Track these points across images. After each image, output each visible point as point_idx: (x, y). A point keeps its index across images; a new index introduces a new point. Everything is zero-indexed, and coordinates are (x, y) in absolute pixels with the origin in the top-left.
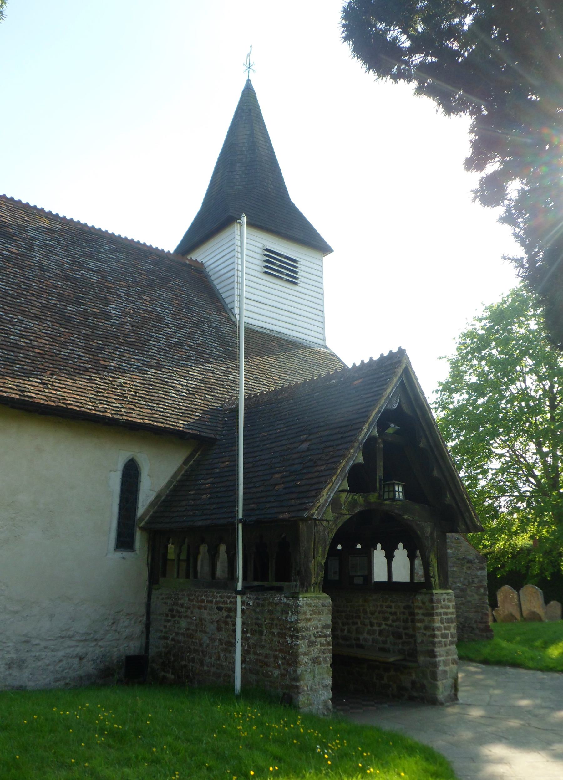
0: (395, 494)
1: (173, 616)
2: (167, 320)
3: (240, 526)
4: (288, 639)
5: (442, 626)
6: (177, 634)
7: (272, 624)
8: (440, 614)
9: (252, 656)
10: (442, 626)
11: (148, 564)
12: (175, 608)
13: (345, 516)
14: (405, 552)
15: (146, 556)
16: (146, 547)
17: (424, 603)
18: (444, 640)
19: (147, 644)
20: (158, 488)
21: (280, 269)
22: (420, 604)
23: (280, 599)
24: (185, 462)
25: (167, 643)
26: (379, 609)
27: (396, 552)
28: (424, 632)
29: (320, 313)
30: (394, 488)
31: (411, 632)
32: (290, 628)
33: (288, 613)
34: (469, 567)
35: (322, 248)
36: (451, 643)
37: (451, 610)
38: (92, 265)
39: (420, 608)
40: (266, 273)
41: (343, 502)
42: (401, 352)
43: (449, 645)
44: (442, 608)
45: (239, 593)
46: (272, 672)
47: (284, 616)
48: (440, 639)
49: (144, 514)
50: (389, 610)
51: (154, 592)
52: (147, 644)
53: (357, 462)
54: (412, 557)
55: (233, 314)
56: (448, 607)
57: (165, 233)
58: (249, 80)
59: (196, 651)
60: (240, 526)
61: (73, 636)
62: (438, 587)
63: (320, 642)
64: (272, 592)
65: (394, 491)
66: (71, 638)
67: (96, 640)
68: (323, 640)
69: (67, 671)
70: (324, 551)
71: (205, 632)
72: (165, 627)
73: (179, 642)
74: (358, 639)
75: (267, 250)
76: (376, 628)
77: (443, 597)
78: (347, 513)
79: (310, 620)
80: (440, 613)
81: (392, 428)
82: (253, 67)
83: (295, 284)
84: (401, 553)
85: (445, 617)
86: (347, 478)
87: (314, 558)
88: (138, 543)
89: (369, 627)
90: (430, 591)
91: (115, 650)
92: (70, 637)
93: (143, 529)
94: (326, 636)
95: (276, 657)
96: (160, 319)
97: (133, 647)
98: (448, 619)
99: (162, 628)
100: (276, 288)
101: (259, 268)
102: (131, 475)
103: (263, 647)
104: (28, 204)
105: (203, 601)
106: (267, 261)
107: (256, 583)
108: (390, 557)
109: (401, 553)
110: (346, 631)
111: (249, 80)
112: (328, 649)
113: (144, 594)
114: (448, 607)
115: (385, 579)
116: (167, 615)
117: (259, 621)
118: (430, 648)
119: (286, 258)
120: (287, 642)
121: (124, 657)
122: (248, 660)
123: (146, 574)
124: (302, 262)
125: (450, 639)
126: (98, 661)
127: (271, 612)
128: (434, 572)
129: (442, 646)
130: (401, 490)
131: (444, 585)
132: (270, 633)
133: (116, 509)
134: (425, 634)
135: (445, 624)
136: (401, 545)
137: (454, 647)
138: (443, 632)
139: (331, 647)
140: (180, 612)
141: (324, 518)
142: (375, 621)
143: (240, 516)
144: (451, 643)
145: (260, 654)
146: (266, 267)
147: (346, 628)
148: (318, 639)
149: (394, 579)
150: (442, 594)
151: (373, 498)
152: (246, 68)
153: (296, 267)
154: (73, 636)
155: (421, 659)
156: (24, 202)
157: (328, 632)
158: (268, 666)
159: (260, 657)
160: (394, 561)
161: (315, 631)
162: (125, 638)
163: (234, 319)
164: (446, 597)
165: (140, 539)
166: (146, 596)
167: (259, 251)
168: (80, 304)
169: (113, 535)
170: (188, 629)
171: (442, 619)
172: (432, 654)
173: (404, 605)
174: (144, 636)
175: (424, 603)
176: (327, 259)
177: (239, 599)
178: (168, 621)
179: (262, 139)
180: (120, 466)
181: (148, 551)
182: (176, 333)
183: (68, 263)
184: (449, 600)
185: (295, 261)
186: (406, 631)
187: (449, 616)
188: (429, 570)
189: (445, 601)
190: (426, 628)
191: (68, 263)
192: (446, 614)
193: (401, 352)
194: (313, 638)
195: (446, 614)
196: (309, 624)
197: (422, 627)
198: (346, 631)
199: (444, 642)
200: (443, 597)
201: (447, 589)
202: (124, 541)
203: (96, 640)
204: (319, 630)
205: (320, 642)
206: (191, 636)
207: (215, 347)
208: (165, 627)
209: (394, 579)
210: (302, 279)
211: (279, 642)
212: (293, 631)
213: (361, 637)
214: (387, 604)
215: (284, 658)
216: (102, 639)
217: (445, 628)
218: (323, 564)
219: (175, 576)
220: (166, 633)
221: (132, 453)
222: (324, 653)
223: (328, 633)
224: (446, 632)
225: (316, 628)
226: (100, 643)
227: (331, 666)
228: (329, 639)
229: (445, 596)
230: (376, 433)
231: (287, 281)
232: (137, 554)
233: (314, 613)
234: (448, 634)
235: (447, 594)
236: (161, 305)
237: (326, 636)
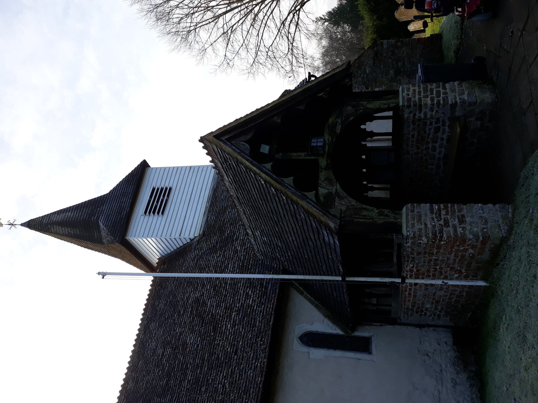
0: (319, 146)
1: (422, 311)
2: (197, 295)
3: (348, 279)
4: (442, 243)
5: (430, 96)
6: (436, 309)
7: (429, 253)
8: (420, 99)
9: (456, 266)
10: (430, 96)
11: (381, 325)
12: (415, 310)
13: (338, 188)
14: (368, 123)
15: (375, 327)
16: (367, 327)
17: (411, 112)
18: (442, 95)
19: (443, 327)
20: (322, 317)
21: (160, 201)
22: (412, 115)
23: (408, 247)
24: (302, 294)
25: (443, 315)
26: (415, 143)
27: (368, 130)
28: (434, 112)
29: (192, 170)
30: (314, 146)
31: (434, 121)
32: (432, 242)
33: (420, 243)
34: (381, 55)
35: (144, 166)
36: (444, 88)
37: (417, 88)
38: (160, 351)
39: (415, 115)
40: (163, 213)
41: (327, 191)
42: (202, 140)
43: (446, 89)
44: (414, 97)
45: (403, 281)
46: (470, 254)
47: (422, 245)
48: (441, 98)
49: (342, 329)
50: (416, 136)
51: (403, 321)
52: (443, 327)
53: (292, 184)
54: (372, 119)
55: (194, 239)
56: (414, 90)
57: (138, 287)
58: (22, 225)
59: (450, 299)
60: (348, 279)
61: (439, 391)
62: (397, 216)
63: (444, 215)
64: (402, 251)
65: (317, 146)
66: (440, 392)
67: (441, 371)
68: (443, 212)
69: (466, 396)
70: (366, 209)
71: (435, 294)
72: (430, 316)
73: (442, 308)
74: (439, 158)
75: (145, 213)
76: (430, 146)
77: (405, 96)
78: (335, 187)
79: (426, 225)
80: (419, 98)
81: (265, 149)
82: (12, 222)
83: (170, 189)
84: (371, 126)
85: (422, 94)
86: (306, 193)
87: (373, 219)
88: (366, 334)
89: (430, 150)
90: (401, 108)
91: (449, 354)
92: (439, 393)
93: (354, 330)
94: (439, 210)
95: (457, 251)
96: (197, 300)
97: (446, 337)
98: (424, 91)
99: (431, 318)
100: (175, 204)
101: (160, 218)
102: (312, 340)
103: (448, 258)
104: (124, 380)
105: (410, 294)
106: (154, 213)
107: (395, 260)
108: (372, 134)
109: (371, 126)
110: (433, 167)
111: (22, 225)
112: (451, 207)
113: (403, 328)
114: (414, 90)
115: (390, 122)
116: (421, 315)
117: (427, 261)
118: (449, 107)
119: (151, 197)
120: (444, 244)
121: (454, 347)
122: (459, 268)
123: (389, 327)
124: (154, 185)
125: (441, 89)
126: (458, 369)
127: (419, 254)
128: (385, 104)
129: (447, 97)
130: (316, 140)
131: (396, 93)
132: (436, 254)
133: (338, 353)
134: (437, 111)
135: (429, 93)
136: (363, 127)
137: (448, 86)
138: (434, 95)
139: (449, 205)
140: (419, 308)
141: (339, 216)
142: (425, 146)
143: (340, 278)
144: (444, 88)
145: (455, 260)
146: (158, 213)
147: (430, 167)
148: (443, 217)
149: (390, 130)
150: (403, 97)
151: (323, 162)
152: (13, 227)
153: (158, 189)
154: (439, 391)
155: (457, 114)
156: (122, 382)
157: (436, 207)
158: (464, 256)
159: (457, 261)
160: (375, 131)
161: (435, 219)
162: (439, 345)
163: (197, 239)
164: (406, 92)
165: (362, 333)
166: (406, 327)
167: (147, 218)
168: (187, 368)
169: (359, 355)
170: (432, 303)
171: (424, 97)
172: (454, 106)
173: (411, 125)
174: (437, 329)
175: (411, 112)
176: (152, 164)
177: (407, 281)
178: (426, 314)
179: (64, 215)
180: (304, 349)
181: (371, 325)
182: (207, 289)
183: (159, 372)
184: (408, 89)
185: (154, 189)
186: (434, 123)
187: (422, 90)
188: (383, 108)
189: (407, 92)
190: (432, 110)
191: (159, 372)
192: (420, 92)
193: (202, 140)
194: (442, 222)
195: (420, 92)
196: (429, 226)
197: (430, 113)
198: (433, 167)
199: (443, 94)
200: (405, 96)
201: (398, 91)
202: (363, 346)
203: (441, 371)
204: (434, 216)
205: (444, 215)
206: (438, 302)
207: (218, 257)
208: (430, 316)
209: (390, 130)
210: (167, 185)
211: (445, 249)
212: (436, 240)
213: (438, 156)
214: (411, 138)
215: (459, 246)
216: (441, 365)
217: (432, 93)
218: (378, 211)
219: (390, 308)
220: (435, 315)
221: (295, 340)
222: (455, 211)
223: (437, 207)
224: (434, 93)
225: (433, 219)
226: (444, 367)
227: (465, 204)
228: (442, 206)
229: (405, 94)
230: (268, 166)
231: (168, 196)
232: (373, 335)
233: (419, 220)
234: (436, 91)
235: (403, 92)
236: (188, 299)
237: (439, 210)
